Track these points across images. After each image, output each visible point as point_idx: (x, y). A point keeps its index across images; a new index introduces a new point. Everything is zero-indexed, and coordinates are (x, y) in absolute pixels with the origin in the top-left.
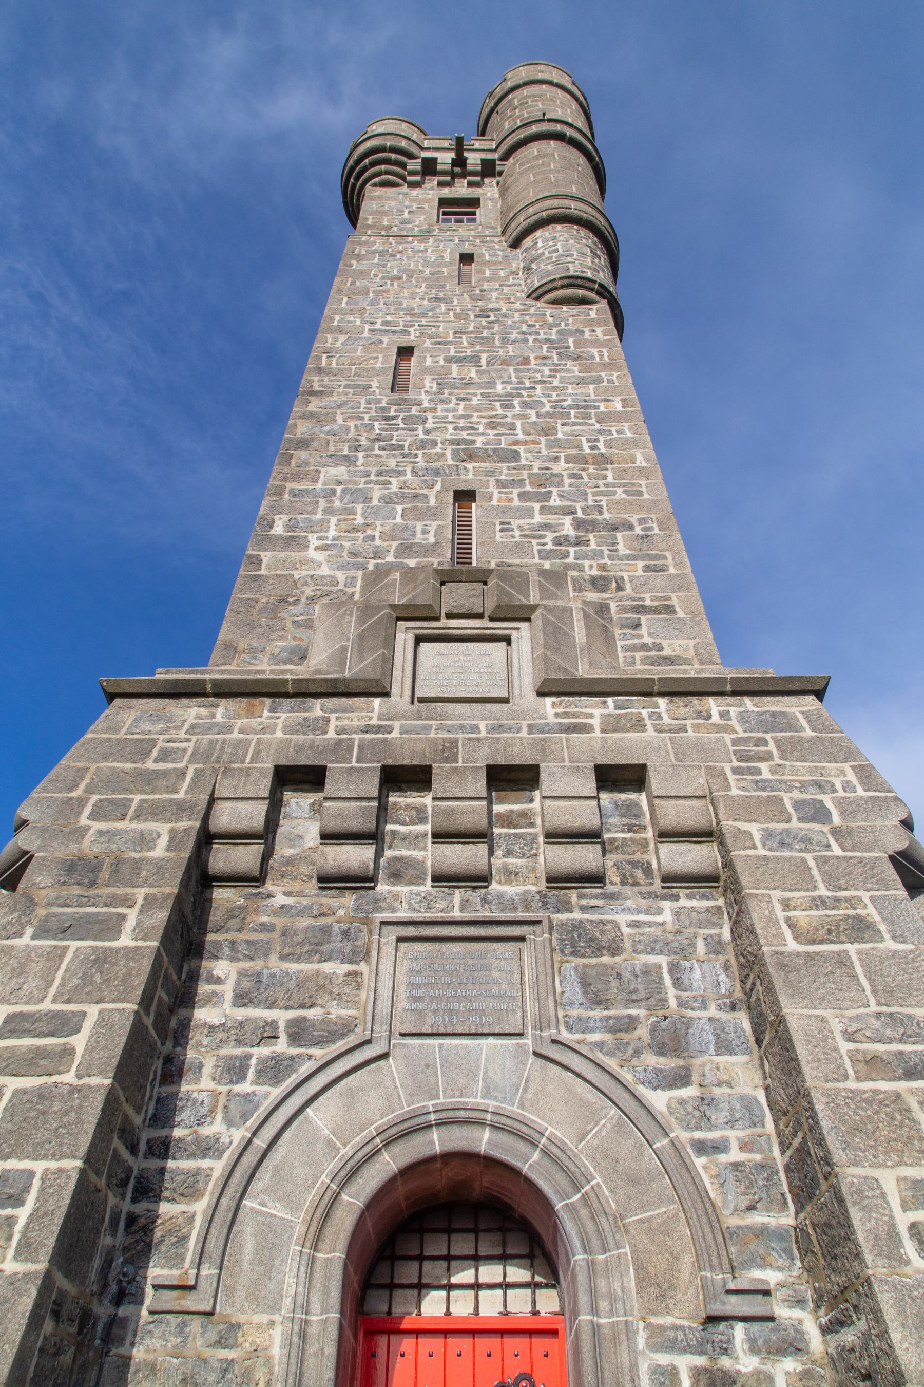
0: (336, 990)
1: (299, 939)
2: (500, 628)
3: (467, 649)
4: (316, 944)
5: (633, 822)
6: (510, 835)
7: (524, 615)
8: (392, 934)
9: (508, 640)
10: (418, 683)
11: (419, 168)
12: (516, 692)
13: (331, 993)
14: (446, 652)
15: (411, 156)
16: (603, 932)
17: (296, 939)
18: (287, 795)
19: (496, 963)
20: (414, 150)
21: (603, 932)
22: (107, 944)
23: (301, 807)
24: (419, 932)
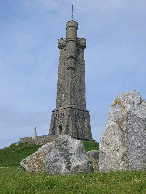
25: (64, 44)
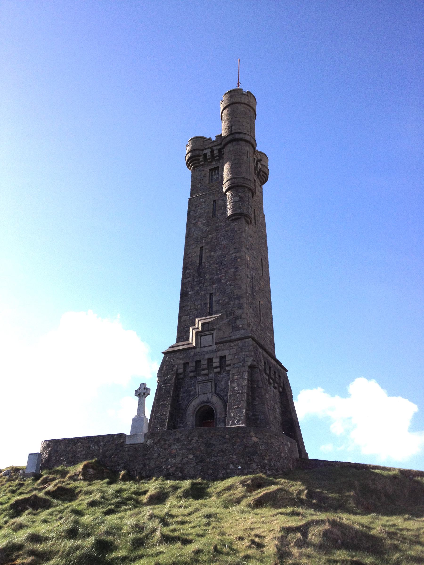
2: (211, 332)
24: (201, 382)
25: (212, 152)
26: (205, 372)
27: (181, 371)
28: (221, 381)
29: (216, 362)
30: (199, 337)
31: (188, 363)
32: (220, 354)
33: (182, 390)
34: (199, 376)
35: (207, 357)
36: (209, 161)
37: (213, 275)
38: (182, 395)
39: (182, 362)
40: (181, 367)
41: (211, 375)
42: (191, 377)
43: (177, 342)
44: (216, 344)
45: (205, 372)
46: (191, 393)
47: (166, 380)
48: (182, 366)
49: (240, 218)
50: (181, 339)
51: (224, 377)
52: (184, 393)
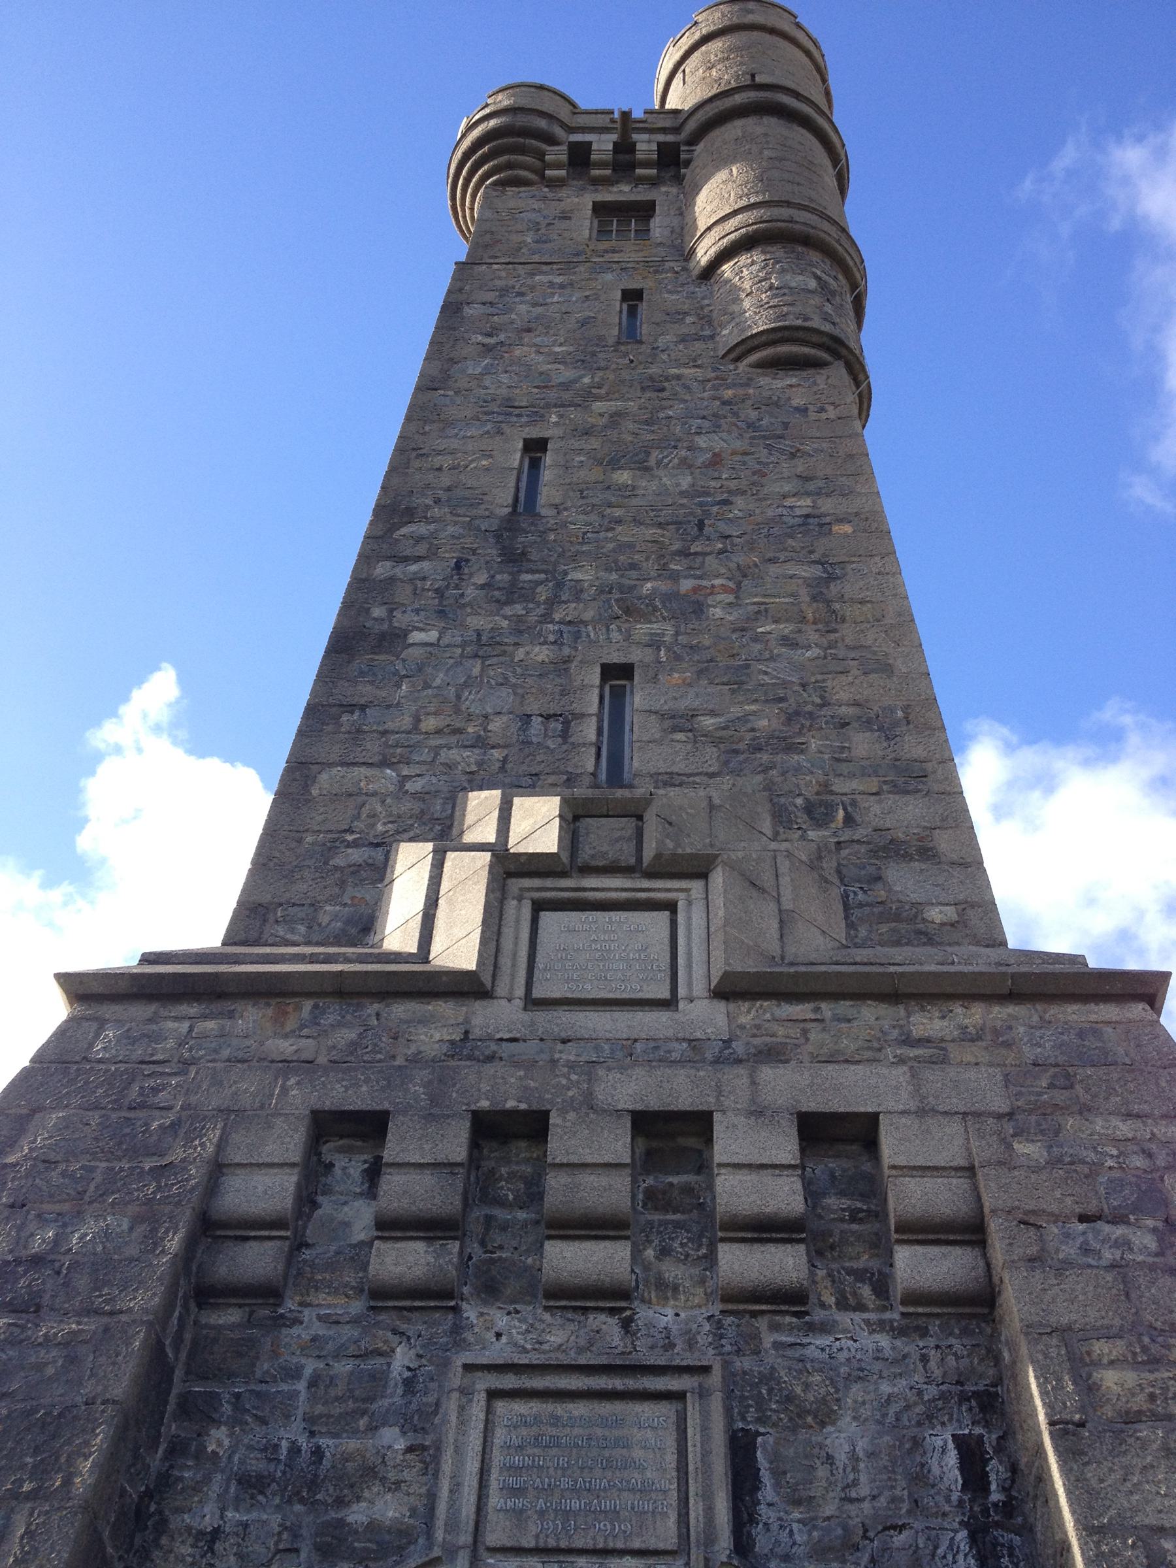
0: (392, 1475)
1: (339, 1390)
2: (661, 888)
3: (611, 922)
4: (364, 1400)
5: (859, 1205)
6: (667, 1222)
7: (698, 869)
8: (485, 1382)
9: (671, 907)
10: (537, 974)
11: (564, 158)
12: (682, 992)
13: (383, 1480)
14: (579, 927)
15: (552, 140)
16: (807, 1386)
17: (333, 1393)
18: (542, 914)
19: (638, 1435)
20: (558, 131)
21: (807, 1386)
22: (496, 162)
23: (349, 1176)
24: (517, 1381)
26: (601, 1260)
27: (264, 1191)
28: (825, 1416)
29: (754, 1165)
30: (518, 913)
31: (370, 1126)
32: (792, 1086)
33: (218, 1439)
34: (490, 1290)
35: (630, 1089)
36: (595, 172)
37: (634, 574)
38: (207, 1517)
39: (300, 1098)
40: (272, 1151)
41: (660, 1316)
42: (383, 1296)
43: (223, 944)
44: (729, 990)
45: (601, 1260)
46: (357, 1515)
47: (37, 1261)
48: (287, 1142)
49: (818, 364)
50: (287, 921)
51: (859, 1375)
52: (252, 1485)
